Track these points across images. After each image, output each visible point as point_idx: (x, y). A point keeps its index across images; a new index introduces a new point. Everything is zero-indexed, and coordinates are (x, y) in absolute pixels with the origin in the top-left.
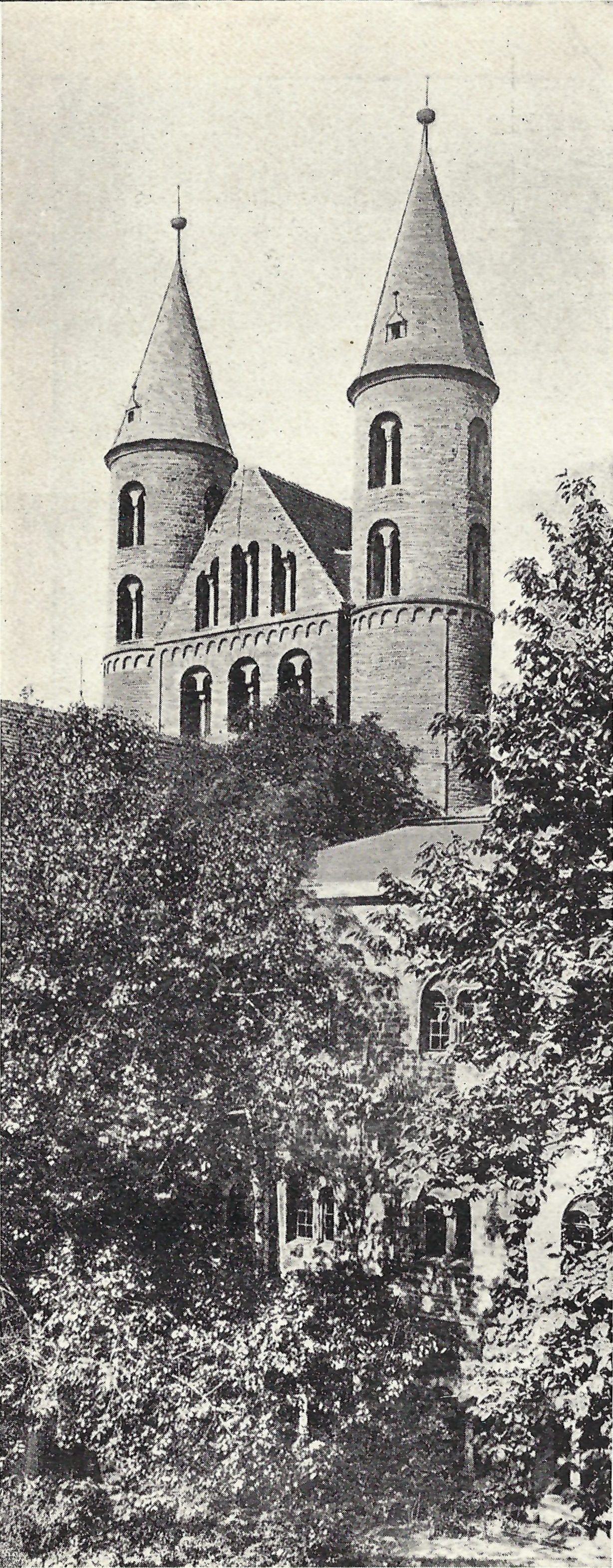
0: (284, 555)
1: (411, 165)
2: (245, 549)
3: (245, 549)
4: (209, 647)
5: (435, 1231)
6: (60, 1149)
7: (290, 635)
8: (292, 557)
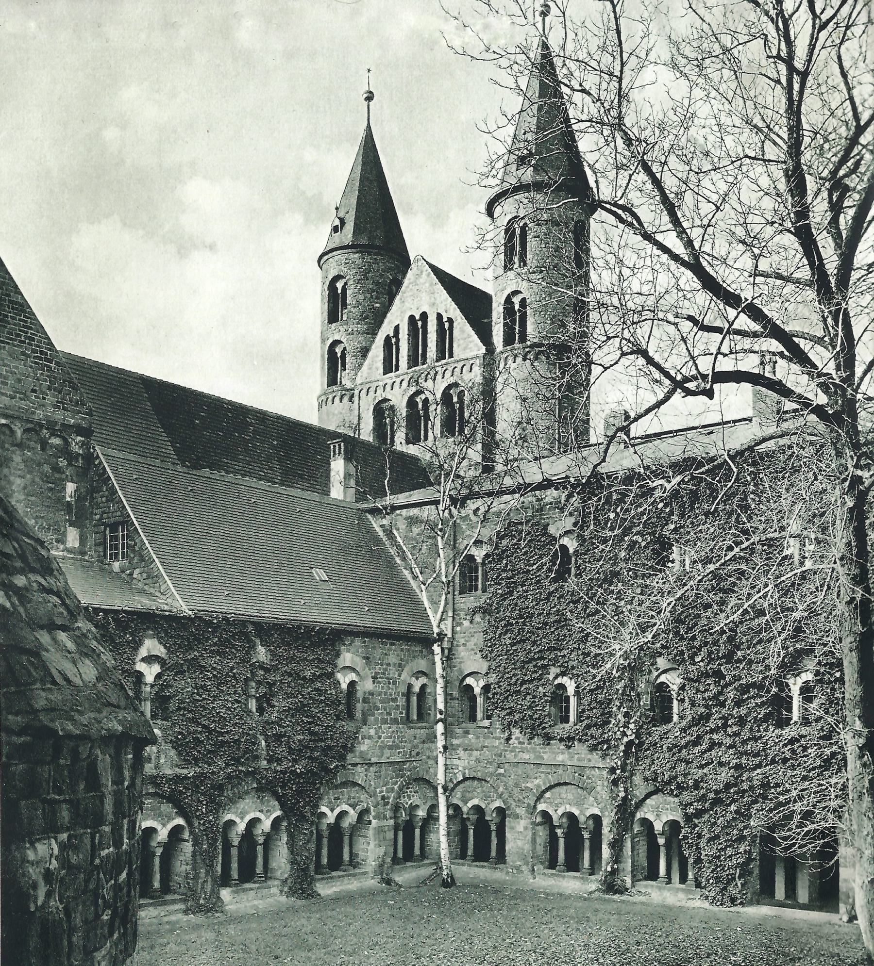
0: (445, 319)
1: (361, 133)
2: (417, 317)
3: (417, 317)
4: (462, 369)
5: (824, 873)
6: (633, 802)
7: (450, 374)
8: (450, 321)
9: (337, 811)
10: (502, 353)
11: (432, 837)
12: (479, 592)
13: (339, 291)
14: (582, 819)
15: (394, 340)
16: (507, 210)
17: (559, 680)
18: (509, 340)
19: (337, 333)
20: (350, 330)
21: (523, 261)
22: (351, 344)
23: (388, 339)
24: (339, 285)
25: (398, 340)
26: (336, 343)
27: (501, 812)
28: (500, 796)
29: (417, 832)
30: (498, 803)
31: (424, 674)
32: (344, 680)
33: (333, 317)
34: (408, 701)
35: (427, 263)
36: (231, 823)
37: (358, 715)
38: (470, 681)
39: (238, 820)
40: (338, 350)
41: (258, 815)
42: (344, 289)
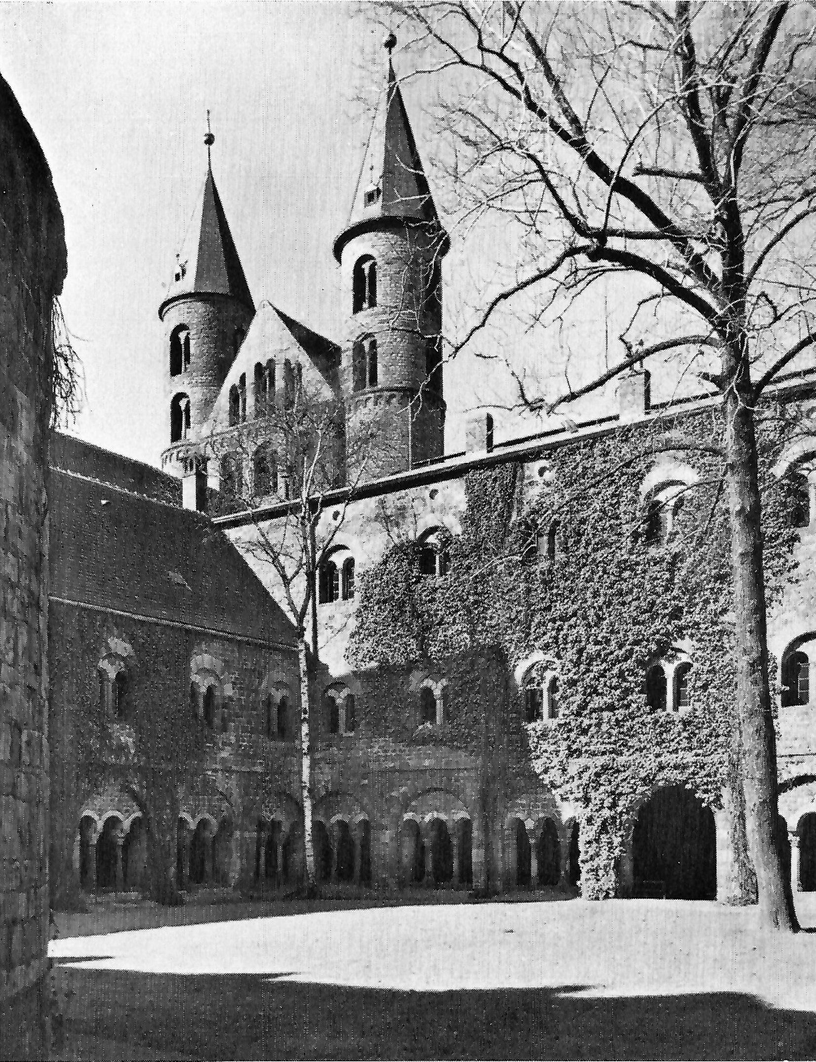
1: (205, 178)
2: (264, 365)
3: (264, 365)
9: (199, 817)
10: (352, 397)
11: (296, 857)
12: (340, 599)
13: (182, 342)
14: (450, 824)
15: (239, 391)
16: (354, 249)
17: (425, 683)
18: (359, 385)
19: (181, 384)
20: (194, 381)
21: (373, 304)
22: (195, 395)
23: (233, 389)
24: (182, 335)
25: (244, 392)
26: (180, 396)
27: (366, 825)
28: (363, 809)
29: (280, 849)
30: (361, 817)
31: (285, 686)
32: (203, 684)
33: (175, 370)
34: (269, 711)
35: (275, 309)
36: (89, 820)
37: (217, 721)
38: (332, 693)
39: (96, 818)
40: (183, 404)
41: (117, 814)
42: (187, 339)
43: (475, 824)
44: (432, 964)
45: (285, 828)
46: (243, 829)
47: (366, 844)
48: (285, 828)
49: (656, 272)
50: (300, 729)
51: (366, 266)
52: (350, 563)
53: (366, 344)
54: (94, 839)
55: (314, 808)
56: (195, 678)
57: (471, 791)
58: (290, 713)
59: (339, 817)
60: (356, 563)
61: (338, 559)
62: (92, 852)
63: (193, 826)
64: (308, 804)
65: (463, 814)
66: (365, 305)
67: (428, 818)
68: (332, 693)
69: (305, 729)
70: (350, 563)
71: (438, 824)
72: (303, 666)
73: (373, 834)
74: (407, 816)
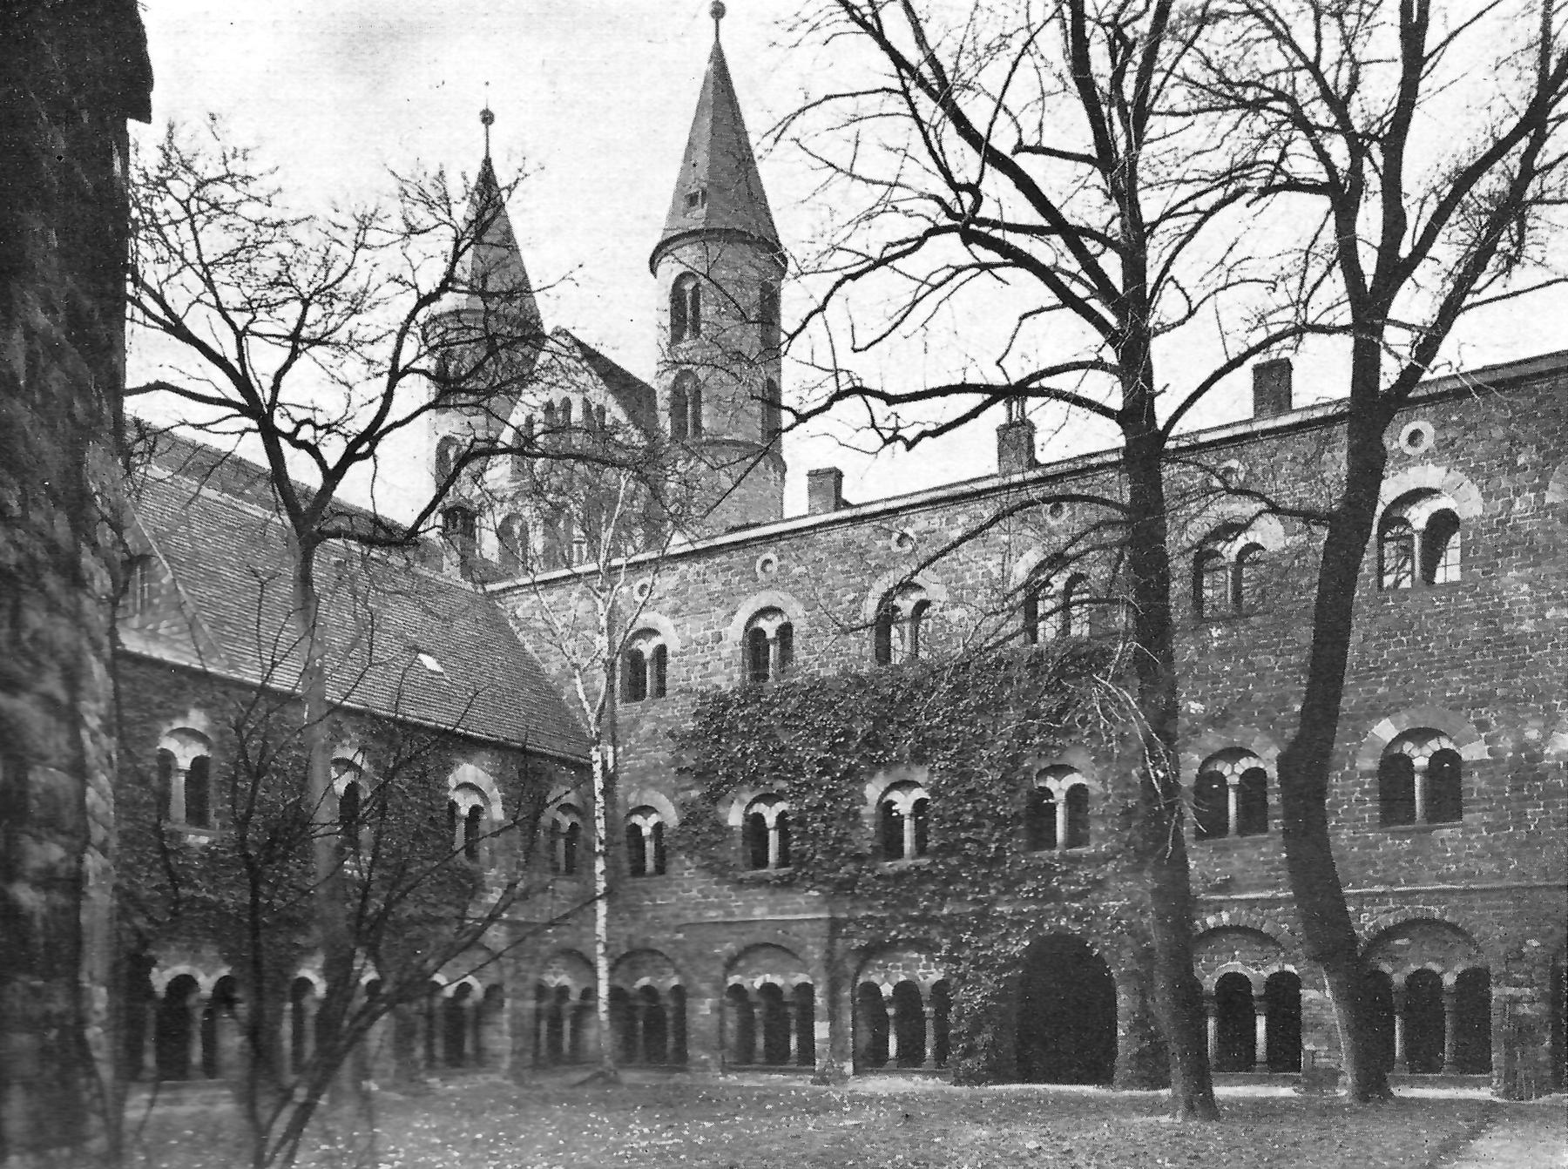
3: (557, 405)
21: (696, 331)
27: (678, 992)
28: (678, 972)
30: (675, 981)
32: (465, 803)
34: (553, 843)
43: (818, 991)
44: (355, 318)
45: (574, 997)
46: (518, 996)
47: (681, 1013)
48: (574, 997)
49: (1046, 274)
50: (593, 866)
51: (689, 286)
52: (661, 651)
53: (688, 384)
54: (313, 1010)
55: (612, 970)
56: (457, 797)
57: (816, 953)
58: (579, 846)
59: (645, 981)
60: (669, 652)
61: (647, 648)
62: (309, 1024)
63: (449, 992)
64: (603, 965)
65: (801, 978)
66: (687, 336)
67: (758, 983)
68: (637, 819)
69: (600, 865)
70: (661, 651)
71: (769, 989)
72: (599, 784)
73: (690, 1003)
74: (733, 980)
